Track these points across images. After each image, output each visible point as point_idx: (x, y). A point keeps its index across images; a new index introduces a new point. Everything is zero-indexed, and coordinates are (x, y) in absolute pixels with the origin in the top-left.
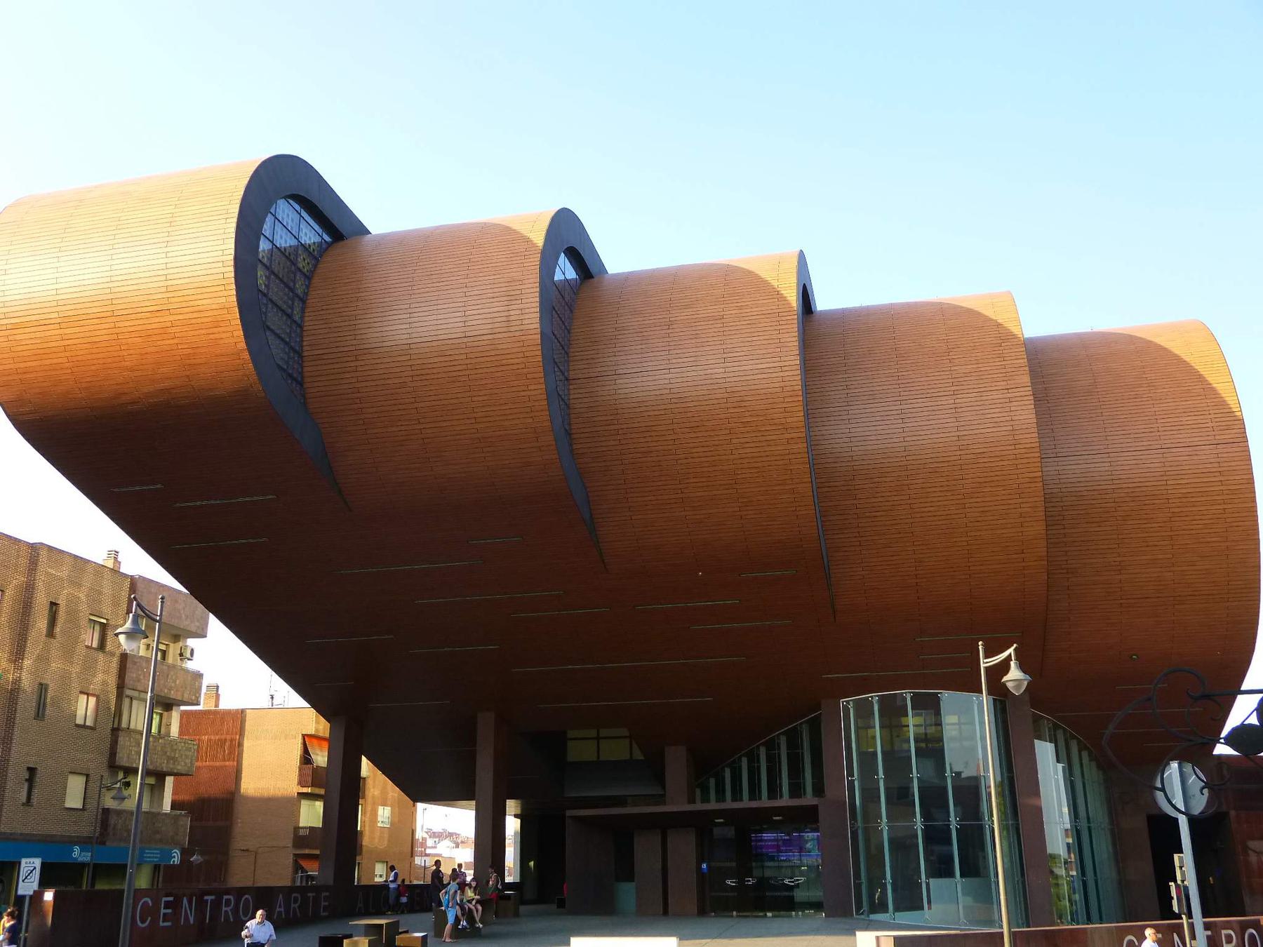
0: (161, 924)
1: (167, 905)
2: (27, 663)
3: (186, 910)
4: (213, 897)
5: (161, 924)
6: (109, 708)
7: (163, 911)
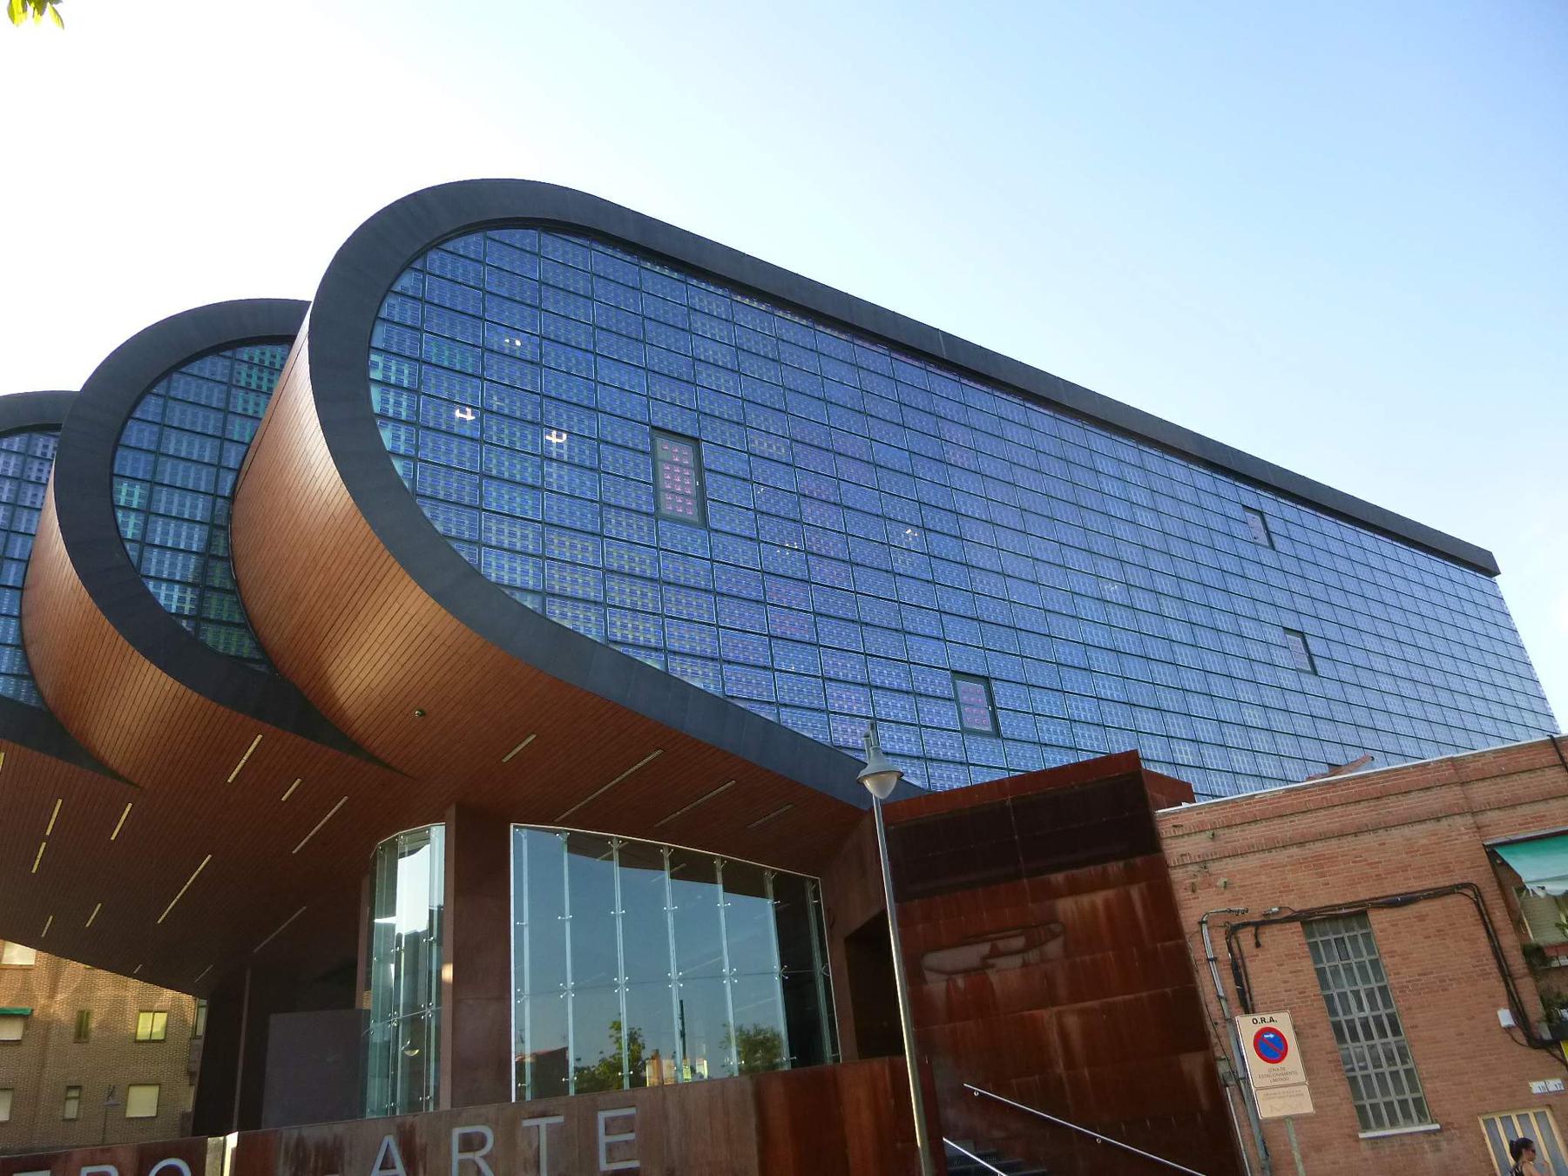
0: (604, 1166)
2: (59, 997)
3: (388, 1145)
4: (559, 1119)
6: (185, 1021)
7: (603, 1140)
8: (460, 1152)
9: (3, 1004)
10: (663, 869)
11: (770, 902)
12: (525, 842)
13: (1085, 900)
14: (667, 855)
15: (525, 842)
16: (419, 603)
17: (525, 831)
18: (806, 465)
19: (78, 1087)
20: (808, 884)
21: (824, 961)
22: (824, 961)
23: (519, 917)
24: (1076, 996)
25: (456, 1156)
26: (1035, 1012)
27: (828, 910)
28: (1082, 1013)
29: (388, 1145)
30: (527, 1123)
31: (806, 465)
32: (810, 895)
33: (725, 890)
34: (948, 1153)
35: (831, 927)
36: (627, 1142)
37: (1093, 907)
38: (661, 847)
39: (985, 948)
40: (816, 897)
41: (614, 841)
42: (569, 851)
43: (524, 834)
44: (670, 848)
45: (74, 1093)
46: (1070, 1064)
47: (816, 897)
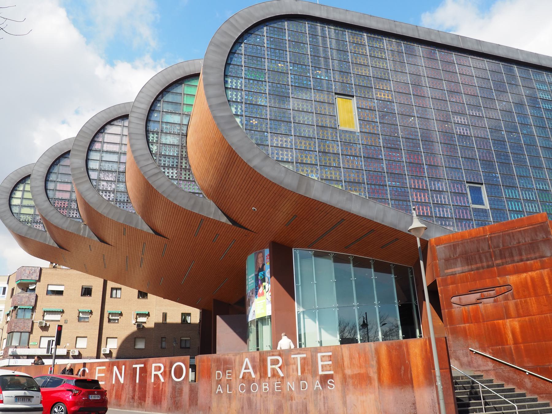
1: (277, 385)
3: (247, 363)
5: (276, 390)
8: (300, 357)
9: (545, 76)
10: (350, 263)
11: (393, 276)
12: (298, 255)
13: (524, 275)
14: (351, 259)
15: (298, 255)
16: (159, 239)
17: (298, 251)
18: (415, 83)
19: (165, 338)
20: (409, 269)
21: (415, 299)
22: (415, 299)
23: (297, 282)
24: (519, 316)
25: (154, 373)
26: (496, 322)
27: (416, 279)
28: (519, 321)
29: (247, 363)
30: (293, 356)
31: (415, 83)
32: (409, 274)
33: (375, 271)
34: (517, 364)
35: (417, 286)
36: (328, 365)
37: (526, 278)
38: (349, 256)
39: (478, 295)
40: (412, 274)
41: (331, 254)
42: (314, 256)
43: (298, 252)
44: (353, 256)
45: (164, 339)
46: (516, 342)
47: (412, 274)
